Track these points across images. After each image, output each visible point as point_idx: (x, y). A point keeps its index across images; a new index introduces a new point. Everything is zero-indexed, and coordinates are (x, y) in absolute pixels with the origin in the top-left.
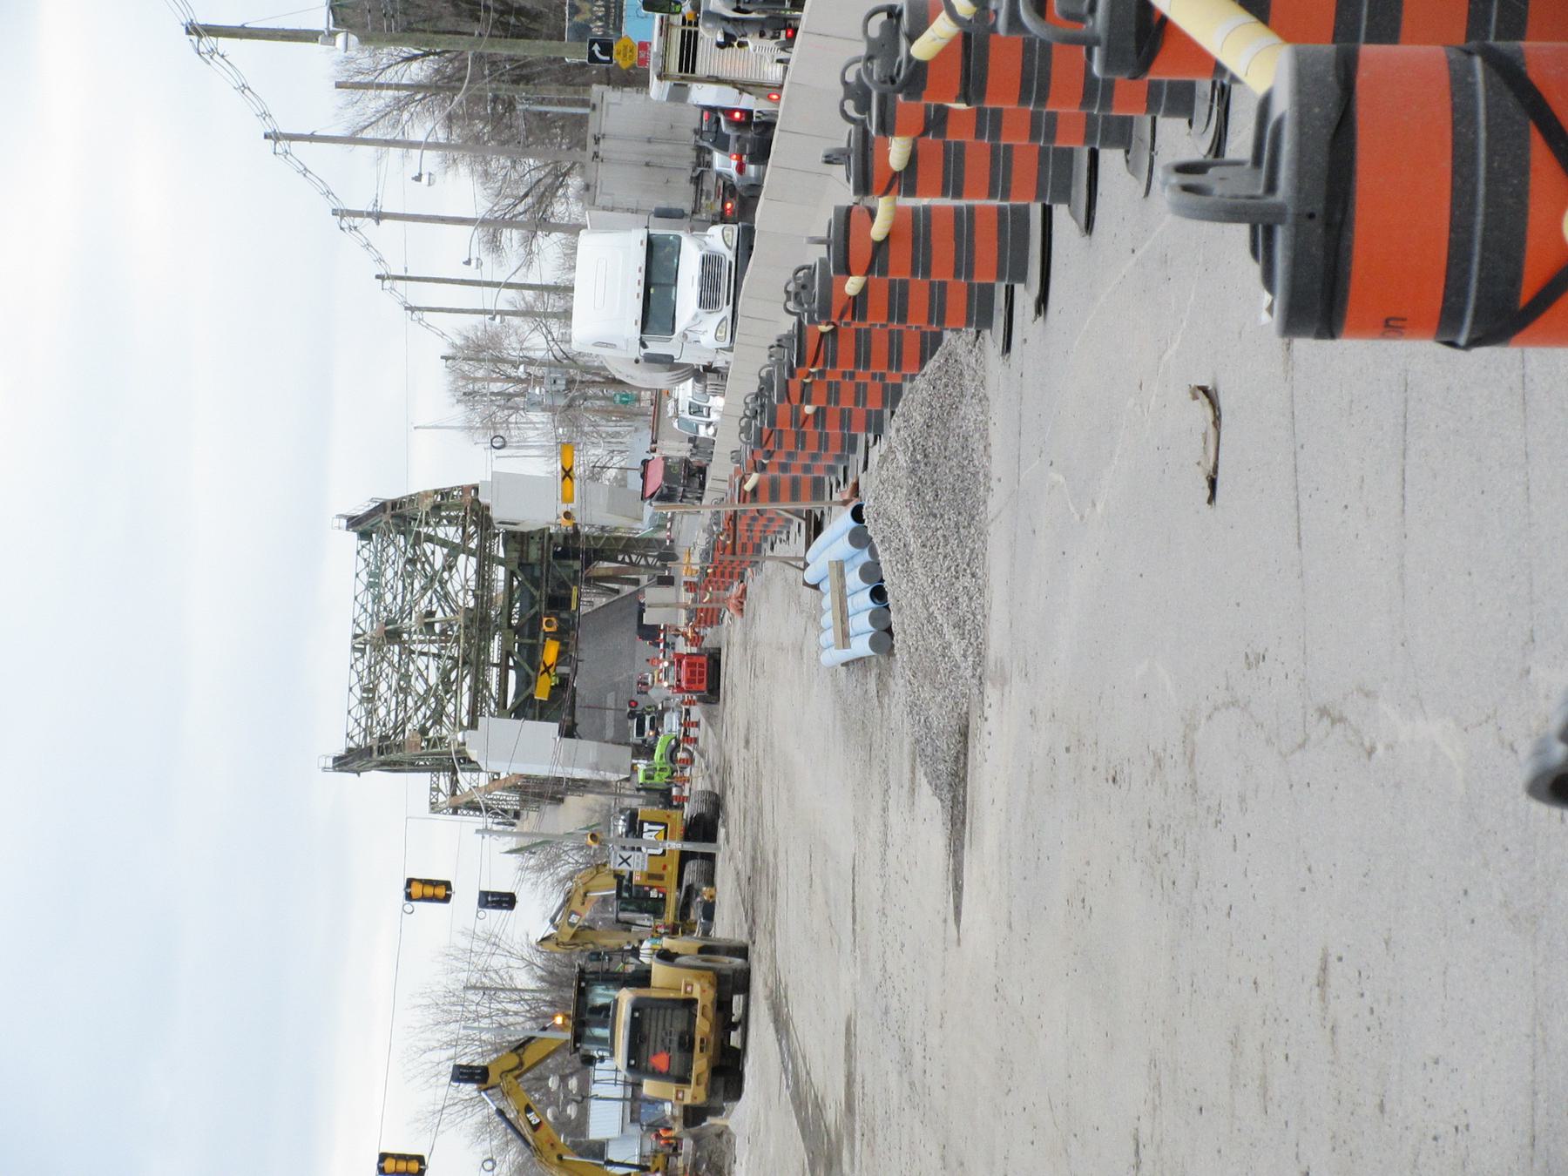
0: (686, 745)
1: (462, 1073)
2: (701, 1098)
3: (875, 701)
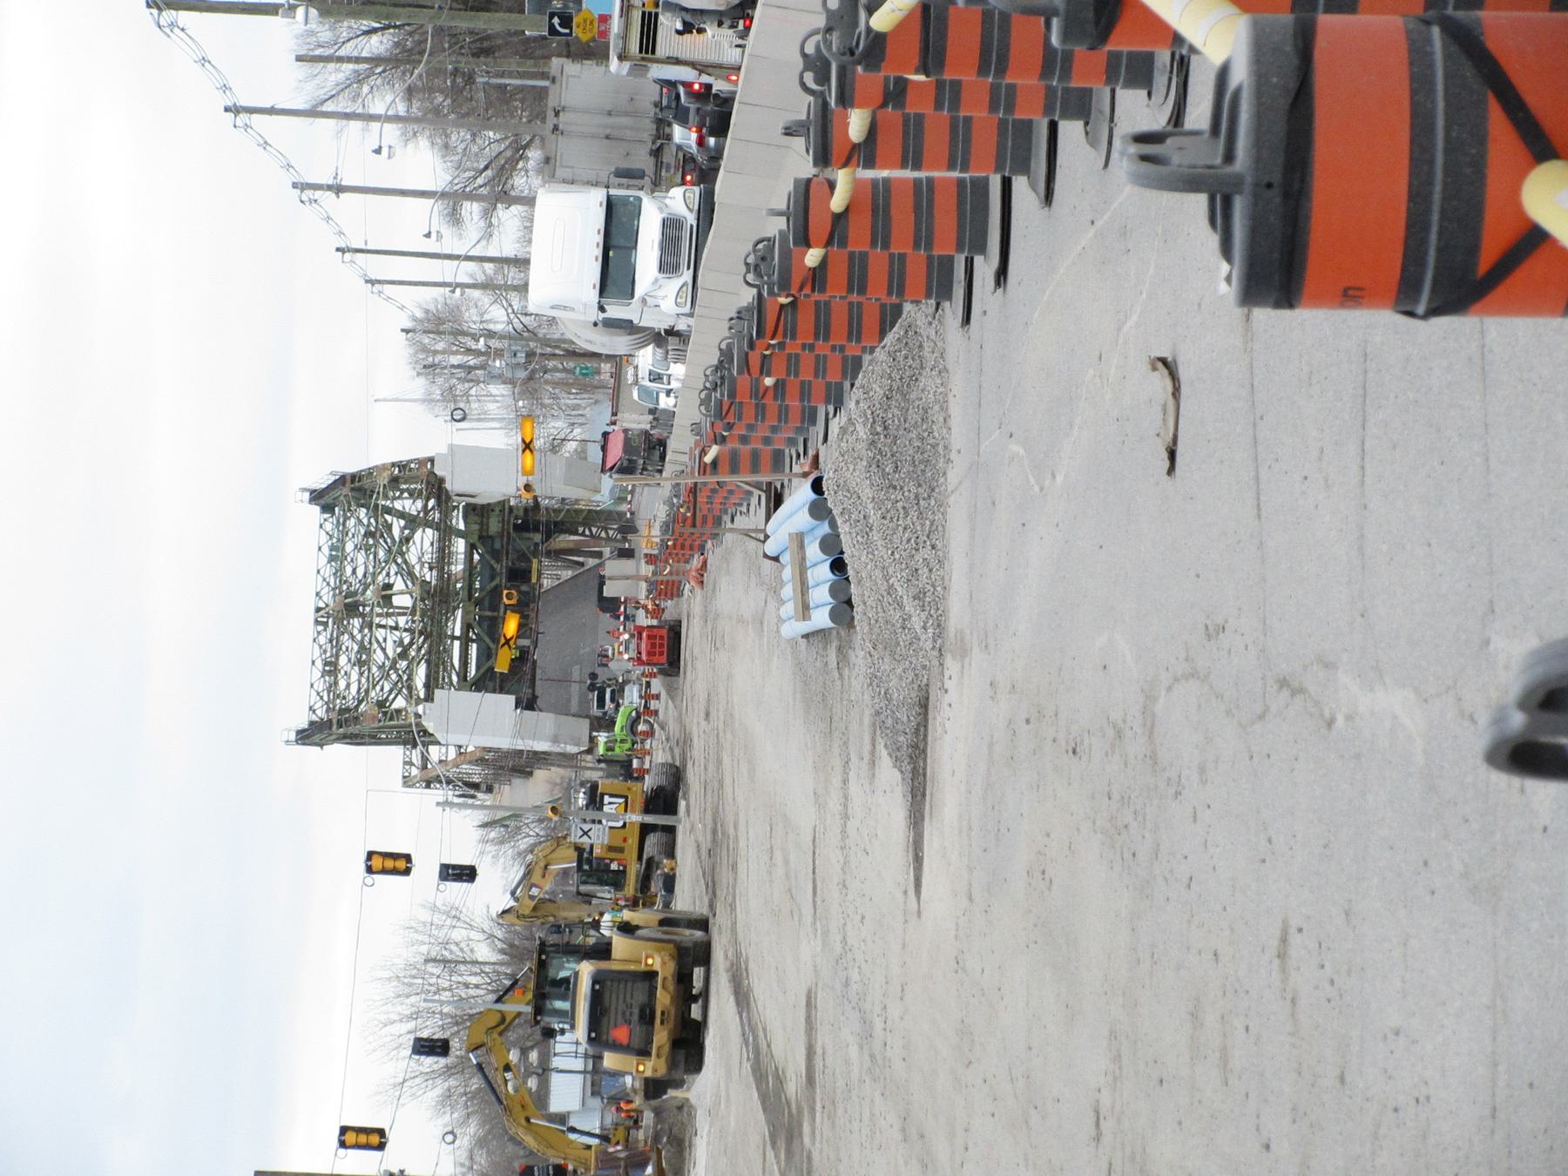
0: (646, 718)
1: (422, 1046)
2: (662, 1070)
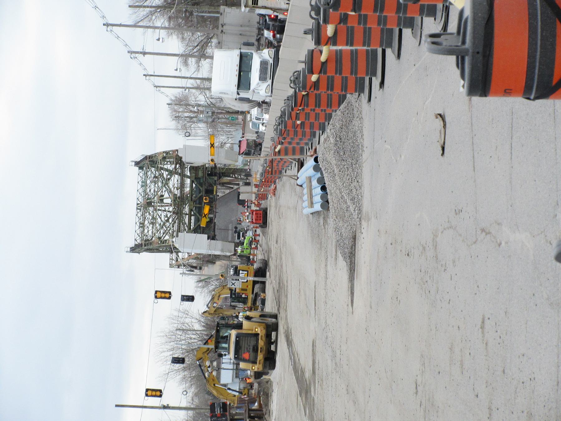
1: (175, 360)
3: (323, 227)
